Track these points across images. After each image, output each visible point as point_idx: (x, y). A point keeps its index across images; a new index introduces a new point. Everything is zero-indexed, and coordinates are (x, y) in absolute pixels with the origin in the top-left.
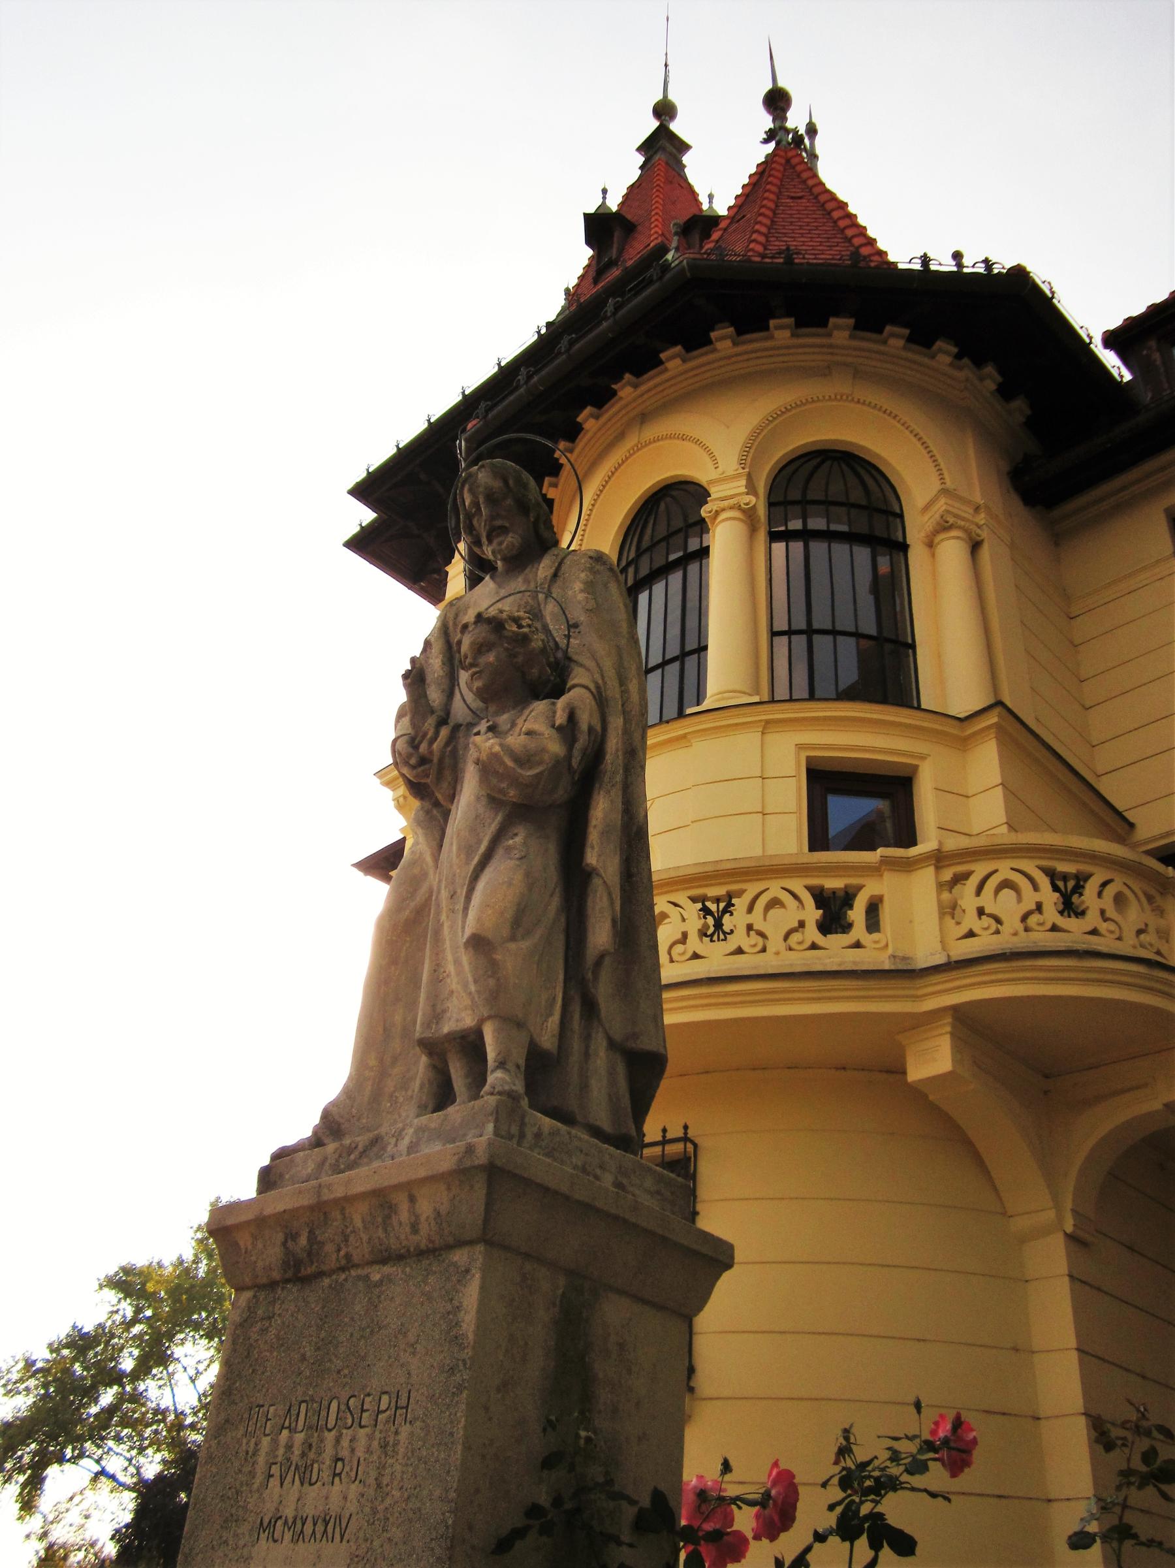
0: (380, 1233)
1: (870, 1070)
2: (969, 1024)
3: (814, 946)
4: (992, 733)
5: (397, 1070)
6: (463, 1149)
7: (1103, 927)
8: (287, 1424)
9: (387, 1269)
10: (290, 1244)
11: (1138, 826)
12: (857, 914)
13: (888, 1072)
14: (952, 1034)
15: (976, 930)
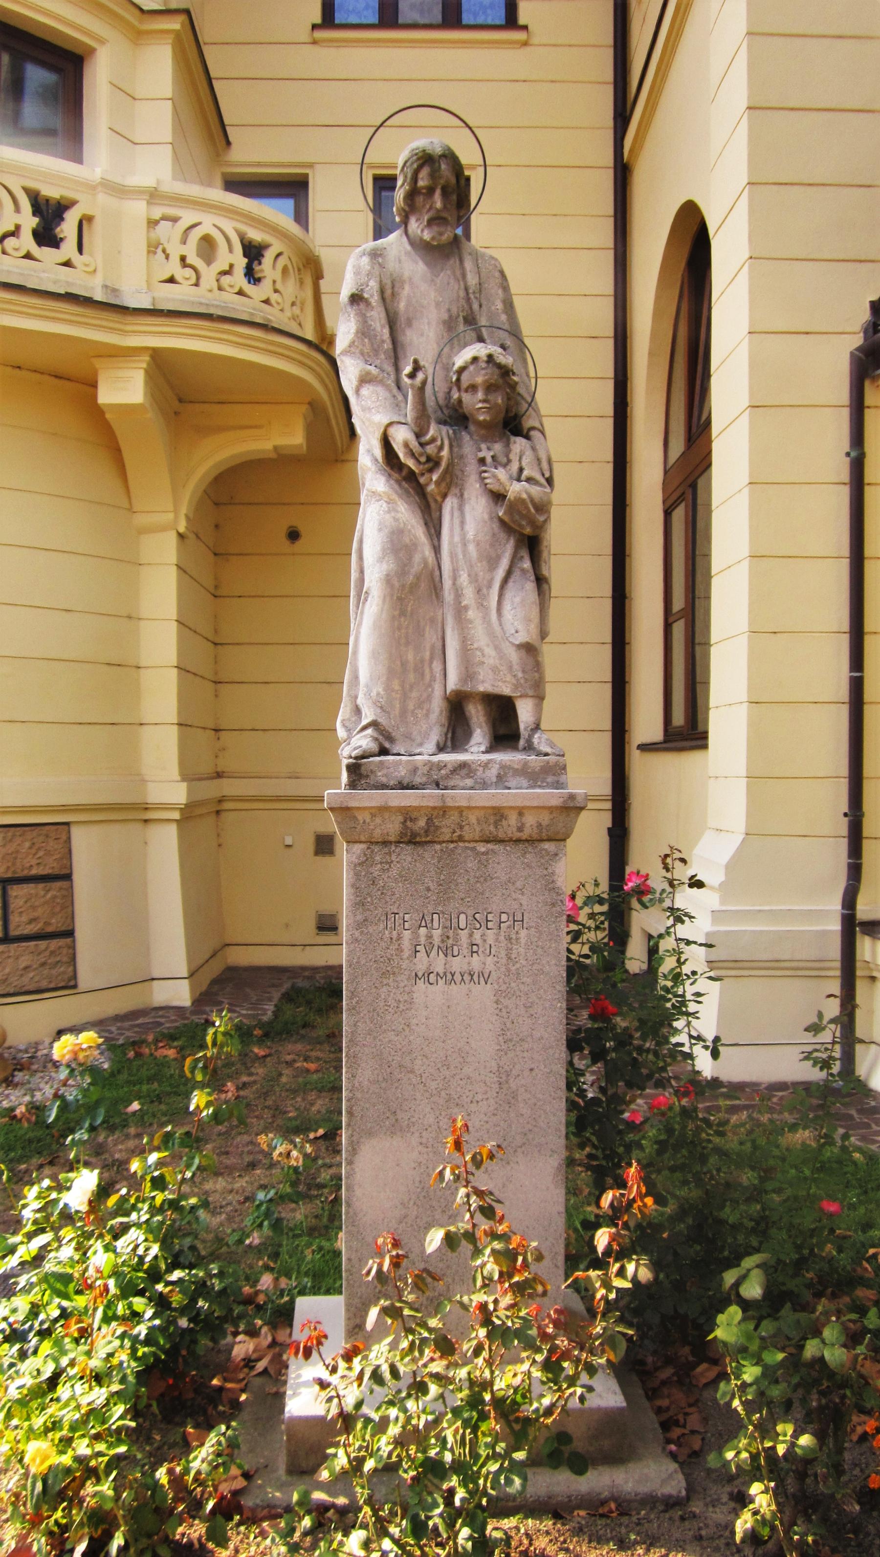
0: (492, 828)
1: (42, 373)
2: (164, 368)
3: (28, 256)
4: (170, 39)
5: (414, 694)
6: (566, 796)
7: (274, 297)
8: (423, 924)
9: (490, 846)
10: (409, 823)
11: (234, 146)
12: (68, 229)
13: (56, 377)
14: (147, 372)
15: (178, 277)
